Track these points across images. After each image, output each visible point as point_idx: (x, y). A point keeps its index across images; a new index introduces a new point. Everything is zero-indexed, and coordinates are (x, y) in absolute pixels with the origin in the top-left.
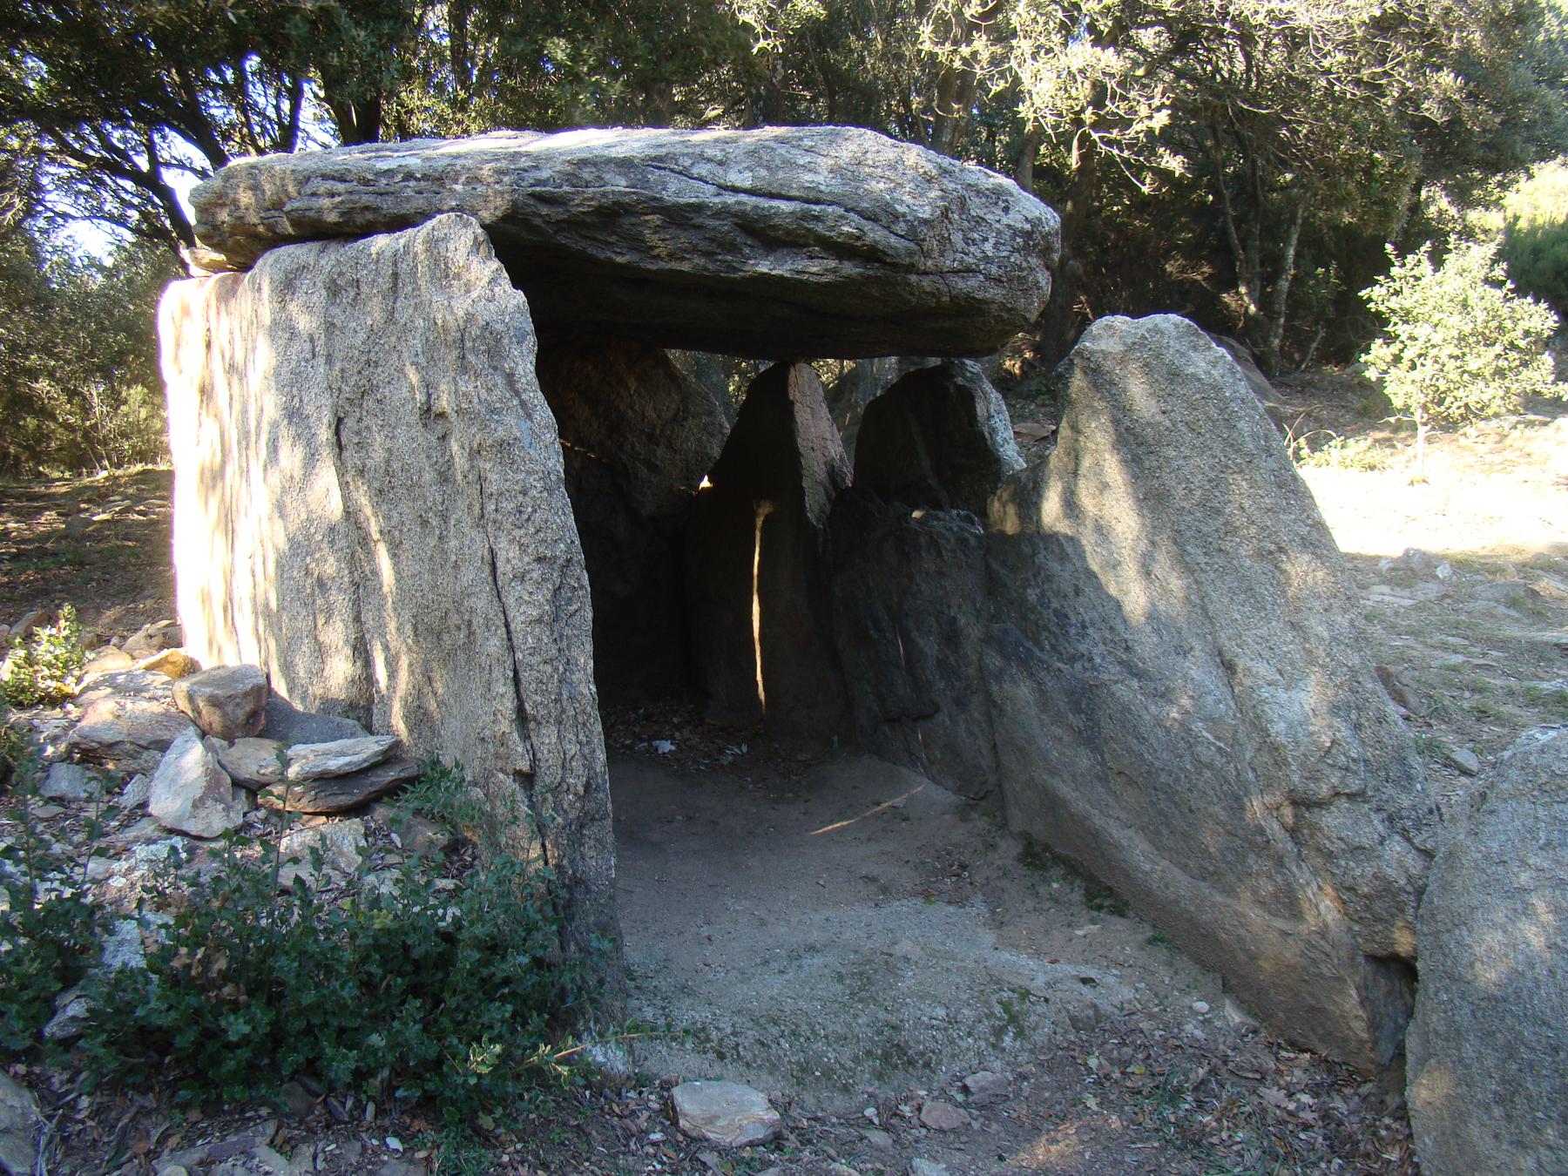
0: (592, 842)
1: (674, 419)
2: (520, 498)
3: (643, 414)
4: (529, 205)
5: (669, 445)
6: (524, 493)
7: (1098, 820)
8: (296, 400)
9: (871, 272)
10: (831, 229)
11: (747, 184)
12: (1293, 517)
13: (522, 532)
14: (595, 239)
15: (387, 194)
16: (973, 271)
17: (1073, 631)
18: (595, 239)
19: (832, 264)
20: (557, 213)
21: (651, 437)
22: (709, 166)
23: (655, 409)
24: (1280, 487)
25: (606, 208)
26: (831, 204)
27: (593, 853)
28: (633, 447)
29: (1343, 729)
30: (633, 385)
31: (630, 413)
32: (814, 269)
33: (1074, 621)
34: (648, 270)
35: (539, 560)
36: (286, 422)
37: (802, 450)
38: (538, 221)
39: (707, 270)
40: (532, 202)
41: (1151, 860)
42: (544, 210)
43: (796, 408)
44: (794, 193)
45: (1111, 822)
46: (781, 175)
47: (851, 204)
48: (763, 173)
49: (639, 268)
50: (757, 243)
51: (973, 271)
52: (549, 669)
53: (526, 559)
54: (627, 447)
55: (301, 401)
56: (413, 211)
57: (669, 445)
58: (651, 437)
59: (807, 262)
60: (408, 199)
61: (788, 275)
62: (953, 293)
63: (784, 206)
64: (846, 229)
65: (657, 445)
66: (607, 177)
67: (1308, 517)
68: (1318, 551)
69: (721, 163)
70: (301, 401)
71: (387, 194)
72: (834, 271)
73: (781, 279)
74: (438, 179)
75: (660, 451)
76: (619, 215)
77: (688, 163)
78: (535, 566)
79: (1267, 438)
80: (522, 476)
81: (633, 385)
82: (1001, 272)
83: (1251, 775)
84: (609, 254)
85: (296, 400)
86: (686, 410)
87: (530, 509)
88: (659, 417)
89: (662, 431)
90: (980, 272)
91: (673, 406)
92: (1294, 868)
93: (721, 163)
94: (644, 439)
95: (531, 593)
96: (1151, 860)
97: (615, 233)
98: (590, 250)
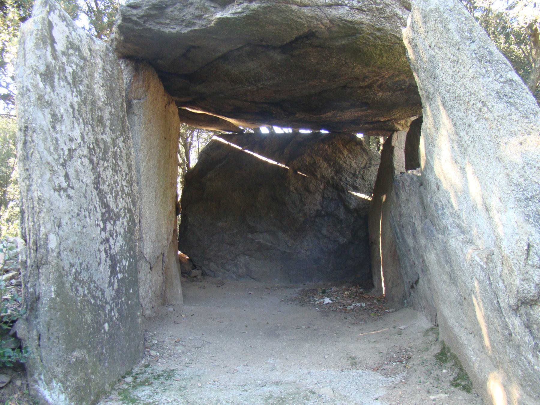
0: (44, 277)
1: (365, 167)
3: (351, 165)
4: (128, 11)
5: (363, 178)
7: (456, 330)
9: (264, 5)
12: (490, 79)
14: (161, 23)
16: (341, 5)
18: (161, 23)
20: (140, 12)
21: (354, 175)
23: (356, 163)
24: (480, 61)
25: (156, 5)
27: (43, 283)
28: (346, 179)
29: (534, 233)
30: (345, 152)
31: (345, 165)
34: (184, 33)
37: (395, 166)
38: (135, 18)
39: (203, 25)
40: (129, 9)
41: (477, 354)
42: (135, 12)
43: (395, 149)
45: (462, 330)
49: (181, 33)
50: (217, 5)
51: (341, 5)
54: (343, 179)
57: (363, 178)
58: (354, 175)
61: (229, 16)
62: (330, 17)
65: (357, 178)
67: (501, 76)
68: (511, 100)
72: (247, 8)
73: (226, 18)
75: (358, 181)
76: (165, 8)
79: (471, 31)
81: (345, 152)
82: (360, 5)
83: (501, 284)
84: (170, 30)
86: (370, 163)
88: (358, 166)
89: (359, 172)
90: (346, 5)
91: (364, 162)
92: (530, 357)
94: (351, 176)
96: (477, 354)
97: (167, 18)
98: (162, 30)
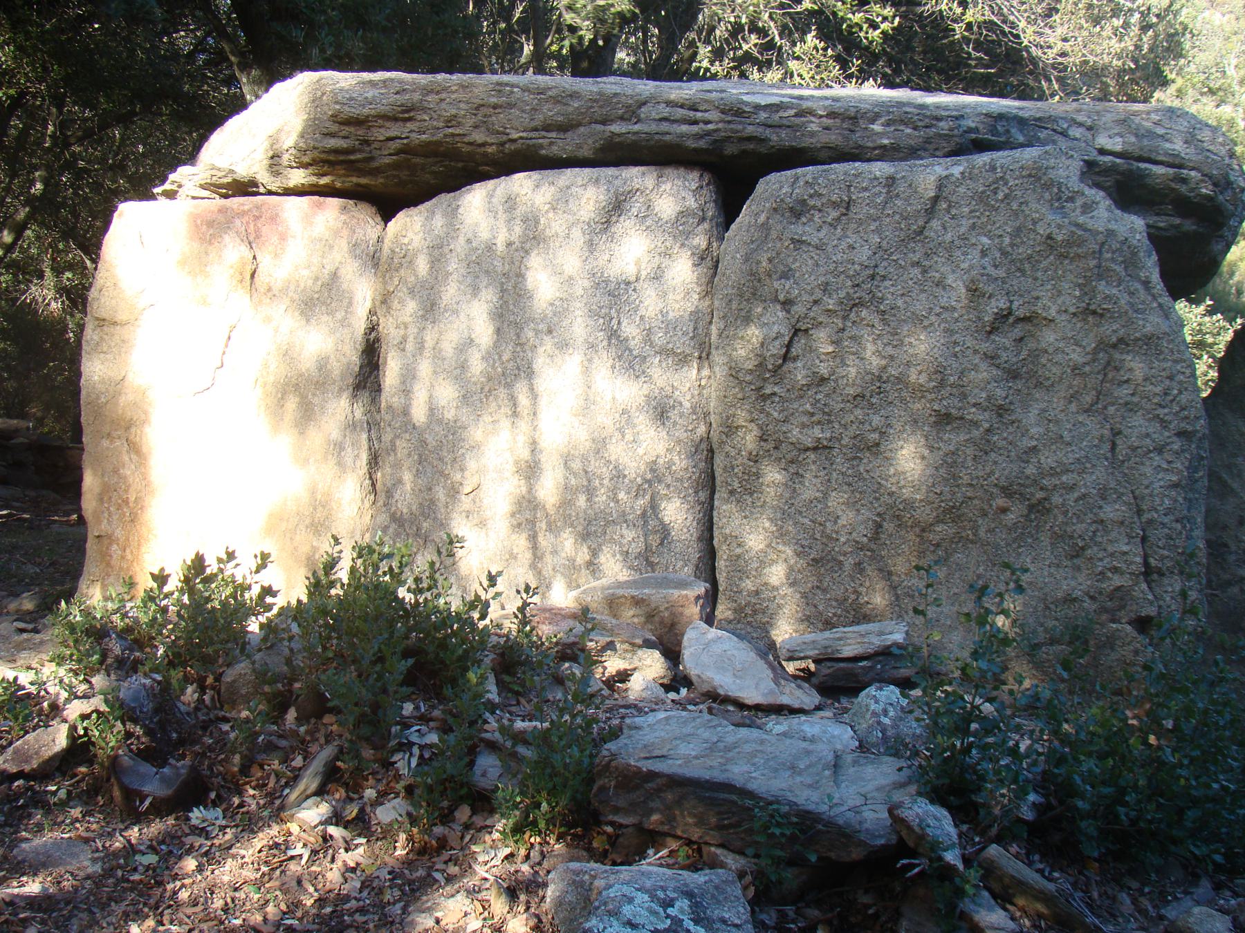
2: (1167, 382)
6: (1171, 378)
8: (615, 322)
10: (1192, 190)
11: (1118, 148)
13: (1166, 411)
15: (780, 127)
17: (1232, 558)
19: (1177, 221)
22: (1081, 130)
26: (1193, 169)
32: (1162, 225)
33: (1233, 548)
35: (1180, 434)
36: (605, 343)
44: (1160, 158)
46: (1145, 142)
47: (1206, 170)
48: (1133, 139)
52: (1179, 526)
53: (1167, 434)
55: (619, 323)
56: (819, 145)
59: (1156, 218)
60: (812, 134)
63: (1160, 170)
64: (1204, 191)
66: (1013, 131)
69: (1090, 129)
70: (619, 323)
71: (780, 127)
72: (1176, 227)
74: (851, 118)
77: (1065, 126)
78: (1175, 439)
80: (1169, 364)
85: (615, 322)
87: (1175, 392)
93: (1090, 129)
95: (1169, 462)
